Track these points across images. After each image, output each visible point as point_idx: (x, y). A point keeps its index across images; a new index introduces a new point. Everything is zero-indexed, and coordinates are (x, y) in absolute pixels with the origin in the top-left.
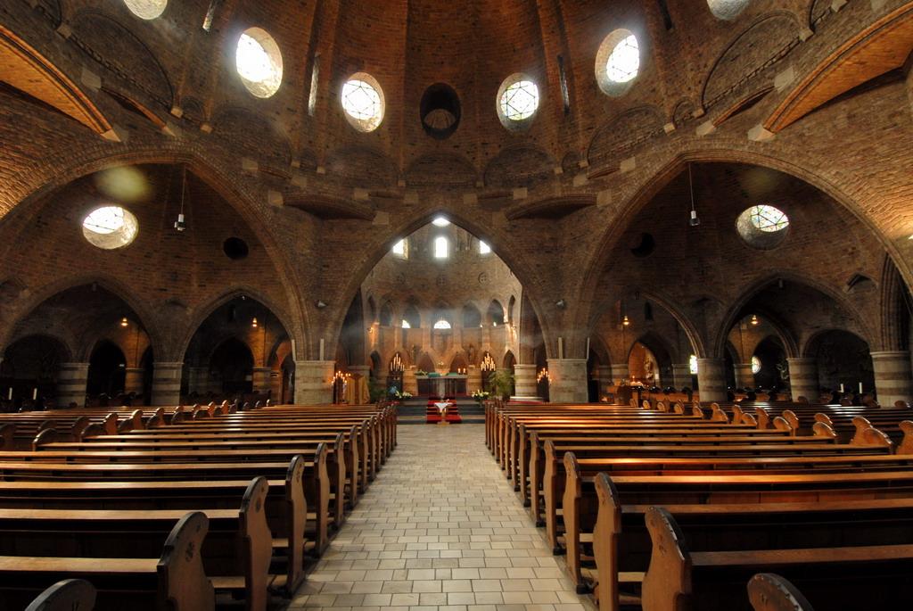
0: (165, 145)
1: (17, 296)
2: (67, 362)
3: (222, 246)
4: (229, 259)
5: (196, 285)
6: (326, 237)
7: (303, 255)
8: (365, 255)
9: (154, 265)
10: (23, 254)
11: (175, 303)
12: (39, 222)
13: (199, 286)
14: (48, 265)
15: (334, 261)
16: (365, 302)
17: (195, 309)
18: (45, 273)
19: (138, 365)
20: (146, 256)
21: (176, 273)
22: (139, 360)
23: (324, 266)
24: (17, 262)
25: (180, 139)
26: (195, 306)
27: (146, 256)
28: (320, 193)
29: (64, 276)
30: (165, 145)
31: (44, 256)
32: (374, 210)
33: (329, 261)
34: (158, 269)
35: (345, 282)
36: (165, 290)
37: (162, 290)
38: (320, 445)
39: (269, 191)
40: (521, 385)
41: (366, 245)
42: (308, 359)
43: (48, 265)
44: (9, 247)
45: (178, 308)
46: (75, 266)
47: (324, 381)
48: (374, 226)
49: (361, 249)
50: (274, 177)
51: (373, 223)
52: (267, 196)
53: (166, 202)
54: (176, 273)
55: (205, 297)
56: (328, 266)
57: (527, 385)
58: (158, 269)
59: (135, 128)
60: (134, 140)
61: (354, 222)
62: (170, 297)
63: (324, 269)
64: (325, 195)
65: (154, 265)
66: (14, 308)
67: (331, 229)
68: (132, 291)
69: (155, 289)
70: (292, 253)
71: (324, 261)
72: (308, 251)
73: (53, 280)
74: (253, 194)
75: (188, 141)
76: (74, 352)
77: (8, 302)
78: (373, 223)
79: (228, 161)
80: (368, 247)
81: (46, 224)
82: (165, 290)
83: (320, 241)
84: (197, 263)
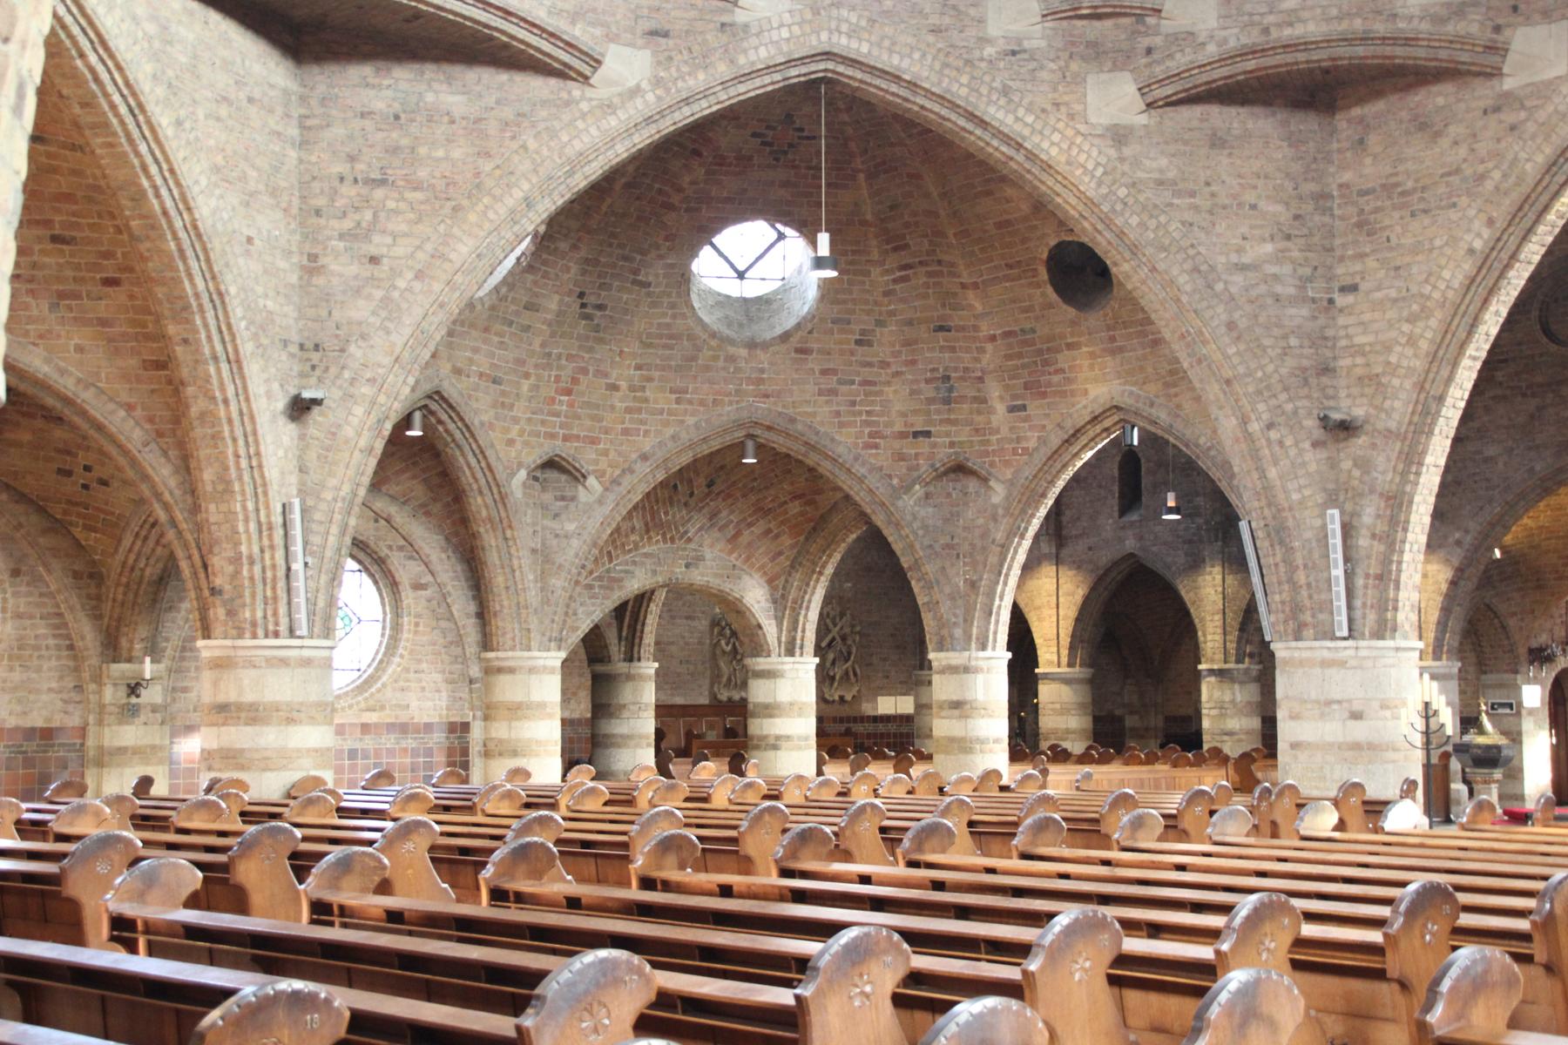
0: (745, 51)
1: (573, 499)
2: (758, 655)
3: (1044, 275)
4: (1071, 312)
5: (1000, 408)
6: (1347, 176)
7: (1242, 268)
8: (1477, 225)
9: (884, 364)
10: (568, 392)
11: (960, 469)
12: (583, 306)
13: (1012, 409)
14: (628, 410)
15: (1371, 263)
16: (245, 560)
17: (1011, 483)
18: (626, 432)
19: (1064, 660)
20: (859, 342)
21: (947, 378)
22: (1065, 640)
23: (1343, 289)
24: (557, 415)
25: (787, 18)
26: (1008, 474)
27: (859, 342)
28: (1266, 31)
29: (670, 431)
30: (745, 51)
31: (614, 388)
32: (1497, 29)
33: (1358, 267)
34: (897, 374)
35: (1412, 341)
36: (928, 434)
37: (916, 434)
38: (1061, 922)
39: (1091, 79)
40: (793, 708)
41: (1481, 178)
42: (1298, 638)
43: (628, 410)
44: (526, 386)
45: (972, 485)
46: (690, 402)
47: (1356, 716)
48: (1507, 95)
49: (1464, 201)
50: (1108, 23)
51: (1508, 84)
52: (1082, 100)
53: (861, 176)
54: (947, 378)
55: (1032, 444)
56: (1353, 288)
57: (770, 710)
58: (897, 374)
59: (666, 35)
60: (667, 69)
61: (1438, 97)
62: (944, 455)
63: (1341, 300)
64: (1287, 32)
65: (884, 364)
66: (571, 527)
67: (1361, 142)
68: (841, 450)
69: (902, 435)
70: (1196, 270)
71: (1340, 270)
72: (1269, 248)
73: (647, 448)
74: (1029, 110)
75: (809, 16)
76: (770, 630)
77: (556, 516)
78: (1508, 84)
79: (935, 30)
80: (1489, 185)
81: (600, 307)
82: (928, 434)
83: (1322, 198)
84: (993, 338)
